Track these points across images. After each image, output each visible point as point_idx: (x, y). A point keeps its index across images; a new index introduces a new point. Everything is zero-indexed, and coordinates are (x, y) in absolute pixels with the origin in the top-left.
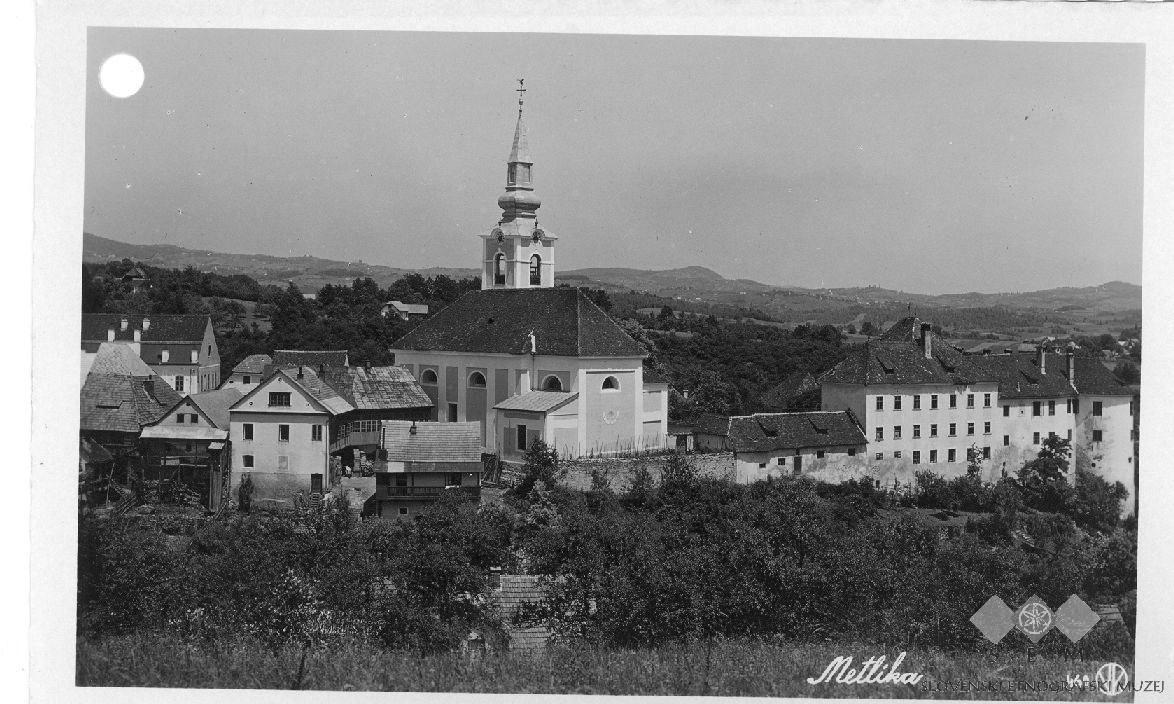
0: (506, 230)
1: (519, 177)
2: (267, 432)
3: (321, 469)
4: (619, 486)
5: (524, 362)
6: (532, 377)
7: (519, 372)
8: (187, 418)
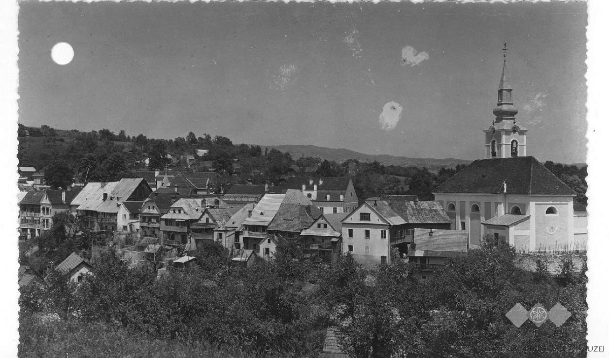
0: (496, 128)
1: (504, 97)
2: (359, 233)
3: (386, 253)
4: (554, 270)
5: (499, 198)
6: (505, 207)
7: (497, 204)
8: (322, 226)
